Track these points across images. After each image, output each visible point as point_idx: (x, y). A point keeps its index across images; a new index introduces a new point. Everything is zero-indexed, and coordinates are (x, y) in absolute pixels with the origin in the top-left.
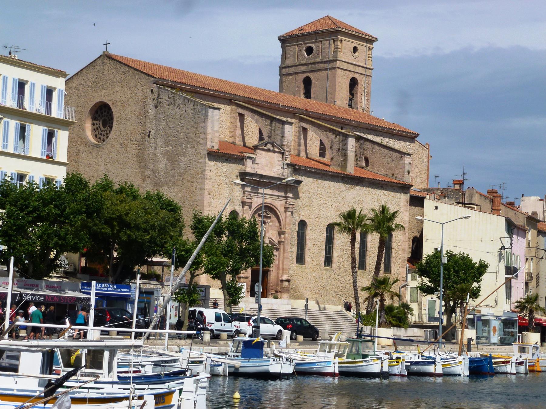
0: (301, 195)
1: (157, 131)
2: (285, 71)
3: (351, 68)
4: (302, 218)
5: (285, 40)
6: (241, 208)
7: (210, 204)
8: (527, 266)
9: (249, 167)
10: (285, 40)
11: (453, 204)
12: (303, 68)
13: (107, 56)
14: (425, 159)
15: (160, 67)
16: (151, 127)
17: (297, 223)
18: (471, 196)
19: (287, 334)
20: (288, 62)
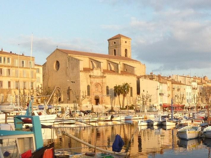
0: (68, 88)
1: (69, 67)
2: (110, 48)
3: (125, 46)
4: (107, 85)
5: (109, 40)
6: (90, 84)
7: (82, 84)
8: (168, 92)
9: (92, 74)
10: (109, 40)
11: (148, 79)
12: (113, 47)
13: (57, 49)
14: (144, 68)
15: (115, 36)
16: (68, 66)
17: (106, 87)
18: (154, 77)
19: (83, 114)
20: (110, 46)
